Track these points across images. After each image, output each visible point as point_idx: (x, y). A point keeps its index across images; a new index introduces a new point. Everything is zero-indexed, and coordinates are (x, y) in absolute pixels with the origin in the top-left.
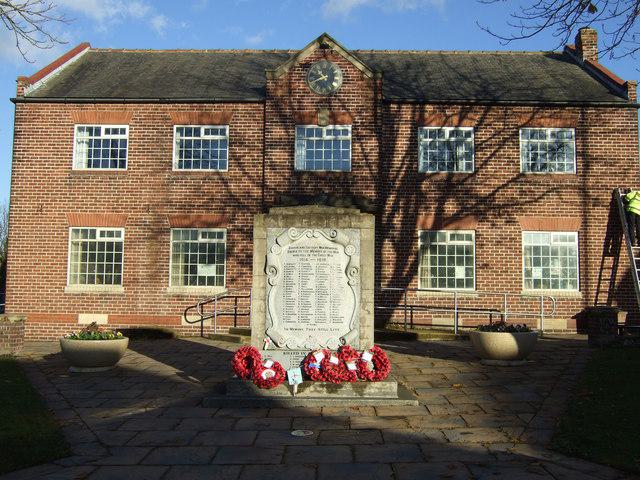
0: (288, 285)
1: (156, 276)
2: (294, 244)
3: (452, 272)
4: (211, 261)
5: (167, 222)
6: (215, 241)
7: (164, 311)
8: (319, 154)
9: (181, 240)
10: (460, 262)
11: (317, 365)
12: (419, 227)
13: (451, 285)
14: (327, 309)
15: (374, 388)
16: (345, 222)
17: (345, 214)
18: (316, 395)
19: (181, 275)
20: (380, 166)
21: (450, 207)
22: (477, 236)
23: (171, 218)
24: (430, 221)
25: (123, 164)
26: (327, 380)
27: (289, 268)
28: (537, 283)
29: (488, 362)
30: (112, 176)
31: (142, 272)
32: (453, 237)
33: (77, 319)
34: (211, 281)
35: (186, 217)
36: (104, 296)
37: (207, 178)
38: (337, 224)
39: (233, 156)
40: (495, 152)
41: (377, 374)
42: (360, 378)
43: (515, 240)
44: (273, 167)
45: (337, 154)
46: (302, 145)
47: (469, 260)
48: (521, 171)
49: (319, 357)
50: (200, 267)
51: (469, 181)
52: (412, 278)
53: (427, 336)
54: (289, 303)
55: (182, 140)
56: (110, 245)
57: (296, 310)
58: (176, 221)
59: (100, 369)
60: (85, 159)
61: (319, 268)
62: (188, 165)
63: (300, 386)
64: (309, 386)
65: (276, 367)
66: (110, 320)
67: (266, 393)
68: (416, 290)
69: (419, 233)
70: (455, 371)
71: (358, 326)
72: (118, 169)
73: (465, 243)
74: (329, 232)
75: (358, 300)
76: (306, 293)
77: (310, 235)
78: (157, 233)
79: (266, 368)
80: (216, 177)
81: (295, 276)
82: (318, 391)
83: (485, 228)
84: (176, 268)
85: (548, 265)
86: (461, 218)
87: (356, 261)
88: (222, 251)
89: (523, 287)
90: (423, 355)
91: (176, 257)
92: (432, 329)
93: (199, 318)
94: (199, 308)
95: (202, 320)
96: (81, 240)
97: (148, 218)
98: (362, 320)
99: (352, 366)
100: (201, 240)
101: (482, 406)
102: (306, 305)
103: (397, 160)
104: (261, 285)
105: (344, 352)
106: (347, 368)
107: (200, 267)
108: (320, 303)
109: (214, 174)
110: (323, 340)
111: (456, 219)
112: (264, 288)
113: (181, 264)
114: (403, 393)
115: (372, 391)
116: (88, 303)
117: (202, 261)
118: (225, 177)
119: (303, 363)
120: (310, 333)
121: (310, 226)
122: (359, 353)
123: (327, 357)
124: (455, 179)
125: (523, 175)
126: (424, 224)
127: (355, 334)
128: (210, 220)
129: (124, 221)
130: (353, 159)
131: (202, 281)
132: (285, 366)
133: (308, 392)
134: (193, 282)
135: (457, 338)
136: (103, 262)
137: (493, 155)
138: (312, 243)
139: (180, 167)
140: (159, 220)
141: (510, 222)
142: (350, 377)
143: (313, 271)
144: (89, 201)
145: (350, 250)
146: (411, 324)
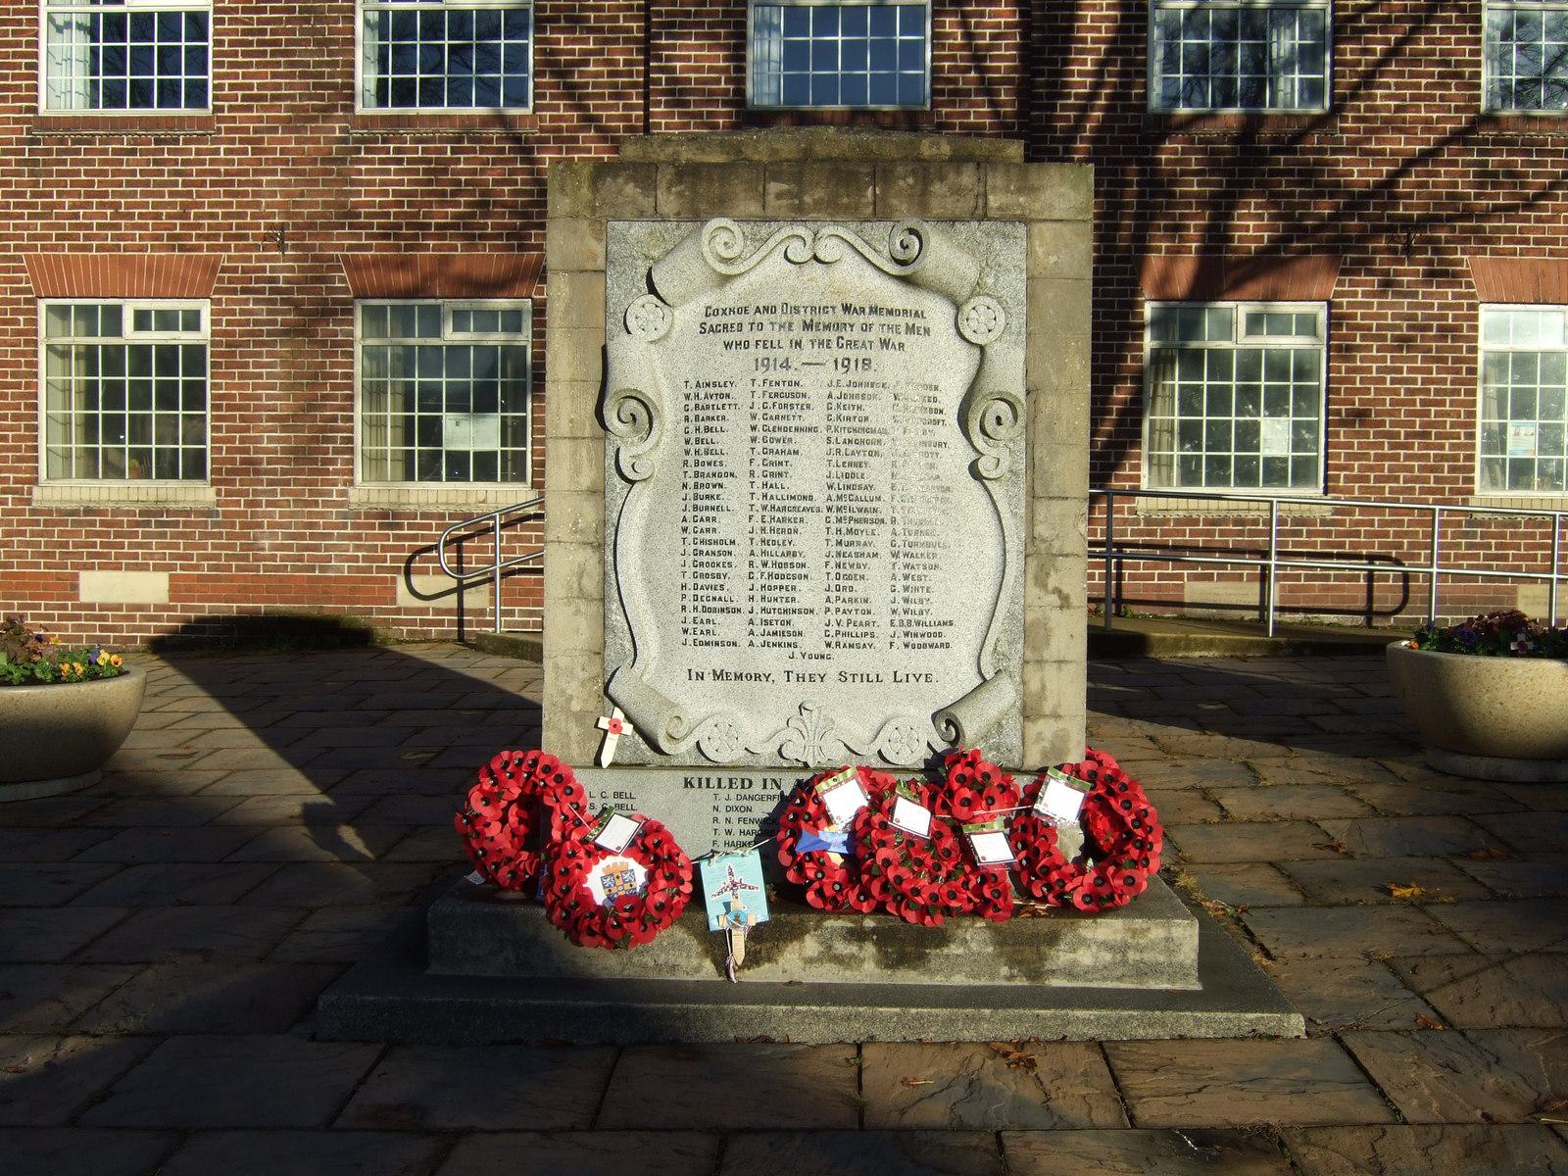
0: (702, 479)
1: (314, 453)
2: (731, 296)
3: (1249, 436)
4: (485, 404)
5: (342, 280)
6: (497, 338)
7: (343, 559)
8: (825, 53)
9: (390, 342)
10: (1276, 407)
11: (834, 840)
12: (1147, 293)
13: (1247, 477)
14: (877, 584)
15: (1091, 949)
16: (957, 191)
17: (958, 160)
18: (828, 974)
19: (391, 447)
20: (1025, 92)
21: (1251, 227)
22: (1335, 320)
23: (355, 266)
24: (1184, 272)
25: (197, 94)
26: (880, 909)
27: (706, 403)
28: (1521, 472)
29: (1463, 763)
30: (165, 133)
31: (269, 441)
32: (1254, 323)
33: (75, 587)
34: (485, 467)
35: (403, 264)
36: (151, 514)
37: (467, 134)
38: (923, 208)
39: (550, 63)
40: (1400, 42)
41: (1102, 878)
42: (1026, 893)
43: (1458, 334)
44: (677, 95)
45: (884, 53)
46: (772, 28)
47: (1305, 396)
48: (1483, 105)
49: (845, 800)
50: (449, 420)
51: (1314, 141)
52: (1122, 456)
53: (1176, 645)
54: (707, 559)
55: (384, 14)
56: (167, 354)
57: (737, 588)
58: (373, 278)
59: (33, 791)
60: (80, 78)
61: (841, 403)
62: (404, 94)
63: (756, 934)
64: (797, 934)
65: (652, 845)
66: (175, 591)
67: (607, 962)
68: (1135, 492)
69: (1148, 310)
70: (1355, 808)
71: (1015, 664)
72: (183, 111)
73: (1292, 343)
74: (885, 238)
75: (1015, 545)
76: (780, 513)
77: (800, 253)
78: (312, 316)
79: (606, 852)
80: (495, 132)
81: (733, 441)
82: (838, 960)
83: (1358, 295)
84: (375, 425)
85: (1182, 424)
86: (1285, 263)
87: (1009, 371)
88: (520, 370)
89: (1477, 486)
90: (1201, 725)
91: (375, 393)
92: (1182, 618)
93: (453, 584)
94: (446, 557)
95: (460, 590)
96: (78, 340)
97: (282, 265)
98: (1033, 634)
99: (992, 847)
100: (450, 336)
101: (1465, 935)
102: (784, 570)
103: (1081, 70)
104: (586, 479)
105: (952, 778)
106: (967, 852)
107: (449, 420)
108: (846, 565)
109: (486, 121)
110: (859, 717)
111: (1265, 269)
112: (598, 492)
113: (391, 413)
114: (1227, 977)
115: (1085, 958)
116: (109, 537)
117: (458, 403)
118: (525, 131)
119: (769, 827)
120: (798, 691)
121: (799, 213)
122: (1021, 782)
123: (880, 801)
124: (1266, 132)
125: (1490, 119)
126: (1166, 279)
127: (1004, 697)
128: (479, 272)
129: (206, 279)
130: (934, 70)
131: (458, 466)
132: (688, 838)
133: (795, 962)
134: (430, 472)
135: (1274, 650)
136: (140, 405)
137: (1393, 53)
138: (812, 287)
139: (382, 101)
140: (317, 273)
141: (1441, 274)
142: (984, 895)
143: (815, 417)
144: (94, 216)
145: (980, 318)
146: (1119, 600)
